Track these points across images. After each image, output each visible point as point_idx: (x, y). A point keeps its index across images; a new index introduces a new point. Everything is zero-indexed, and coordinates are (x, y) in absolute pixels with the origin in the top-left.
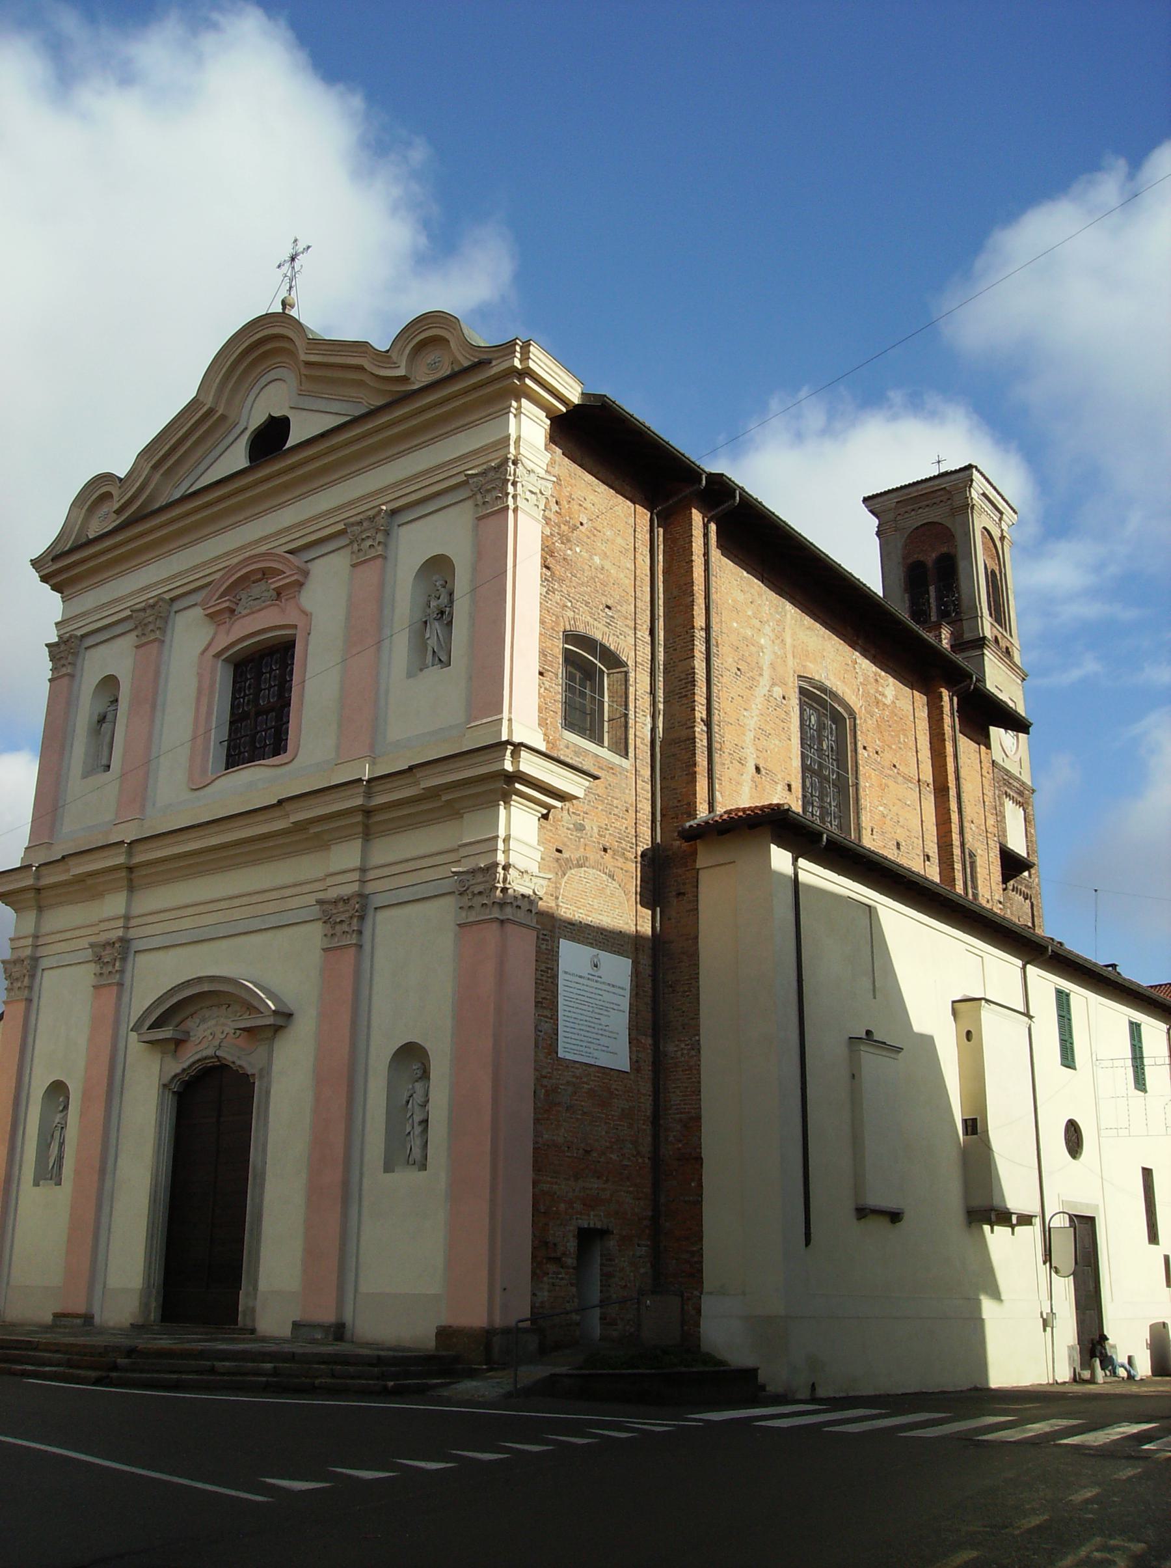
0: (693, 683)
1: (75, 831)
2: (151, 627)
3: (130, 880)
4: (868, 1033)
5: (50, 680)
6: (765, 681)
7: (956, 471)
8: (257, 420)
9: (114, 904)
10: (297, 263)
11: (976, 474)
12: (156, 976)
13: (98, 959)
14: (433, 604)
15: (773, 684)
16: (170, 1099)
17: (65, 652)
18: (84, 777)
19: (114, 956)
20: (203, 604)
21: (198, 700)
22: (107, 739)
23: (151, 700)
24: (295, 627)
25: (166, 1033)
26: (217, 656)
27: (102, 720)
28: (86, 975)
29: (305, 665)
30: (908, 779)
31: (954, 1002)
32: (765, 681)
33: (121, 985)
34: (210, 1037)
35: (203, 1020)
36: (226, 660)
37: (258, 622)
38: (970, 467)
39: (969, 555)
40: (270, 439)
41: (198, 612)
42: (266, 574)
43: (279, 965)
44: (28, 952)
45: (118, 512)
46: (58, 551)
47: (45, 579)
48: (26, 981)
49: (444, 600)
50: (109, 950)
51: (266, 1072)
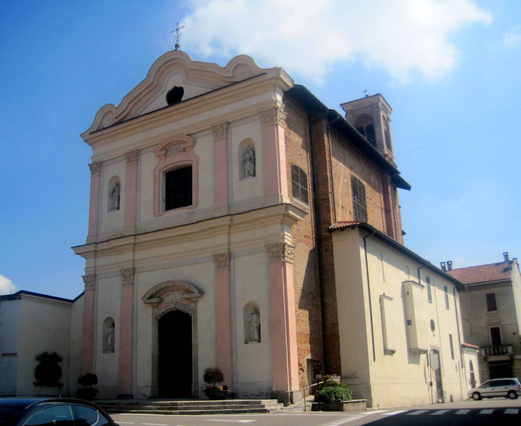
0: (327, 180)
1: (106, 231)
2: (133, 159)
3: (134, 248)
4: (384, 294)
5: (91, 177)
6: (342, 178)
7: (374, 96)
8: (170, 88)
9: (128, 256)
10: (179, 32)
11: (381, 98)
12: (146, 282)
13: (123, 275)
14: (247, 155)
15: (344, 179)
16: (156, 323)
17: (96, 167)
18: (108, 212)
19: (129, 275)
20: (155, 152)
21: (155, 185)
22: (117, 198)
23: (135, 184)
24: (192, 161)
25: (153, 300)
26: (160, 170)
27: (114, 191)
28: (118, 281)
29: (198, 174)
30: (378, 207)
31: (403, 282)
32: (342, 178)
33: (133, 284)
34: (172, 301)
35: (168, 295)
36: (163, 172)
37: (176, 160)
38: (378, 94)
39: (380, 125)
40: (175, 96)
41: (151, 154)
42: (178, 143)
43: (204, 275)
44: (92, 273)
45: (116, 118)
46: (91, 131)
47: (86, 141)
48: (93, 283)
49: (251, 153)
50: (127, 272)
51: (195, 312)
